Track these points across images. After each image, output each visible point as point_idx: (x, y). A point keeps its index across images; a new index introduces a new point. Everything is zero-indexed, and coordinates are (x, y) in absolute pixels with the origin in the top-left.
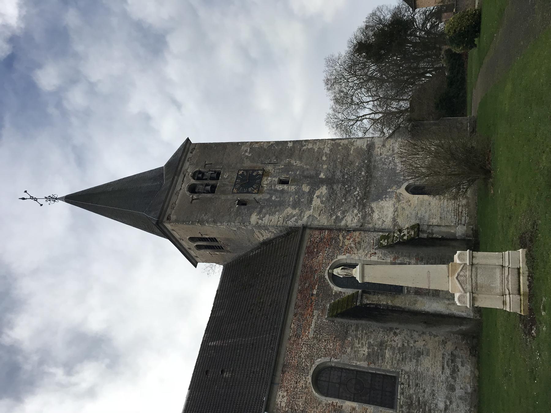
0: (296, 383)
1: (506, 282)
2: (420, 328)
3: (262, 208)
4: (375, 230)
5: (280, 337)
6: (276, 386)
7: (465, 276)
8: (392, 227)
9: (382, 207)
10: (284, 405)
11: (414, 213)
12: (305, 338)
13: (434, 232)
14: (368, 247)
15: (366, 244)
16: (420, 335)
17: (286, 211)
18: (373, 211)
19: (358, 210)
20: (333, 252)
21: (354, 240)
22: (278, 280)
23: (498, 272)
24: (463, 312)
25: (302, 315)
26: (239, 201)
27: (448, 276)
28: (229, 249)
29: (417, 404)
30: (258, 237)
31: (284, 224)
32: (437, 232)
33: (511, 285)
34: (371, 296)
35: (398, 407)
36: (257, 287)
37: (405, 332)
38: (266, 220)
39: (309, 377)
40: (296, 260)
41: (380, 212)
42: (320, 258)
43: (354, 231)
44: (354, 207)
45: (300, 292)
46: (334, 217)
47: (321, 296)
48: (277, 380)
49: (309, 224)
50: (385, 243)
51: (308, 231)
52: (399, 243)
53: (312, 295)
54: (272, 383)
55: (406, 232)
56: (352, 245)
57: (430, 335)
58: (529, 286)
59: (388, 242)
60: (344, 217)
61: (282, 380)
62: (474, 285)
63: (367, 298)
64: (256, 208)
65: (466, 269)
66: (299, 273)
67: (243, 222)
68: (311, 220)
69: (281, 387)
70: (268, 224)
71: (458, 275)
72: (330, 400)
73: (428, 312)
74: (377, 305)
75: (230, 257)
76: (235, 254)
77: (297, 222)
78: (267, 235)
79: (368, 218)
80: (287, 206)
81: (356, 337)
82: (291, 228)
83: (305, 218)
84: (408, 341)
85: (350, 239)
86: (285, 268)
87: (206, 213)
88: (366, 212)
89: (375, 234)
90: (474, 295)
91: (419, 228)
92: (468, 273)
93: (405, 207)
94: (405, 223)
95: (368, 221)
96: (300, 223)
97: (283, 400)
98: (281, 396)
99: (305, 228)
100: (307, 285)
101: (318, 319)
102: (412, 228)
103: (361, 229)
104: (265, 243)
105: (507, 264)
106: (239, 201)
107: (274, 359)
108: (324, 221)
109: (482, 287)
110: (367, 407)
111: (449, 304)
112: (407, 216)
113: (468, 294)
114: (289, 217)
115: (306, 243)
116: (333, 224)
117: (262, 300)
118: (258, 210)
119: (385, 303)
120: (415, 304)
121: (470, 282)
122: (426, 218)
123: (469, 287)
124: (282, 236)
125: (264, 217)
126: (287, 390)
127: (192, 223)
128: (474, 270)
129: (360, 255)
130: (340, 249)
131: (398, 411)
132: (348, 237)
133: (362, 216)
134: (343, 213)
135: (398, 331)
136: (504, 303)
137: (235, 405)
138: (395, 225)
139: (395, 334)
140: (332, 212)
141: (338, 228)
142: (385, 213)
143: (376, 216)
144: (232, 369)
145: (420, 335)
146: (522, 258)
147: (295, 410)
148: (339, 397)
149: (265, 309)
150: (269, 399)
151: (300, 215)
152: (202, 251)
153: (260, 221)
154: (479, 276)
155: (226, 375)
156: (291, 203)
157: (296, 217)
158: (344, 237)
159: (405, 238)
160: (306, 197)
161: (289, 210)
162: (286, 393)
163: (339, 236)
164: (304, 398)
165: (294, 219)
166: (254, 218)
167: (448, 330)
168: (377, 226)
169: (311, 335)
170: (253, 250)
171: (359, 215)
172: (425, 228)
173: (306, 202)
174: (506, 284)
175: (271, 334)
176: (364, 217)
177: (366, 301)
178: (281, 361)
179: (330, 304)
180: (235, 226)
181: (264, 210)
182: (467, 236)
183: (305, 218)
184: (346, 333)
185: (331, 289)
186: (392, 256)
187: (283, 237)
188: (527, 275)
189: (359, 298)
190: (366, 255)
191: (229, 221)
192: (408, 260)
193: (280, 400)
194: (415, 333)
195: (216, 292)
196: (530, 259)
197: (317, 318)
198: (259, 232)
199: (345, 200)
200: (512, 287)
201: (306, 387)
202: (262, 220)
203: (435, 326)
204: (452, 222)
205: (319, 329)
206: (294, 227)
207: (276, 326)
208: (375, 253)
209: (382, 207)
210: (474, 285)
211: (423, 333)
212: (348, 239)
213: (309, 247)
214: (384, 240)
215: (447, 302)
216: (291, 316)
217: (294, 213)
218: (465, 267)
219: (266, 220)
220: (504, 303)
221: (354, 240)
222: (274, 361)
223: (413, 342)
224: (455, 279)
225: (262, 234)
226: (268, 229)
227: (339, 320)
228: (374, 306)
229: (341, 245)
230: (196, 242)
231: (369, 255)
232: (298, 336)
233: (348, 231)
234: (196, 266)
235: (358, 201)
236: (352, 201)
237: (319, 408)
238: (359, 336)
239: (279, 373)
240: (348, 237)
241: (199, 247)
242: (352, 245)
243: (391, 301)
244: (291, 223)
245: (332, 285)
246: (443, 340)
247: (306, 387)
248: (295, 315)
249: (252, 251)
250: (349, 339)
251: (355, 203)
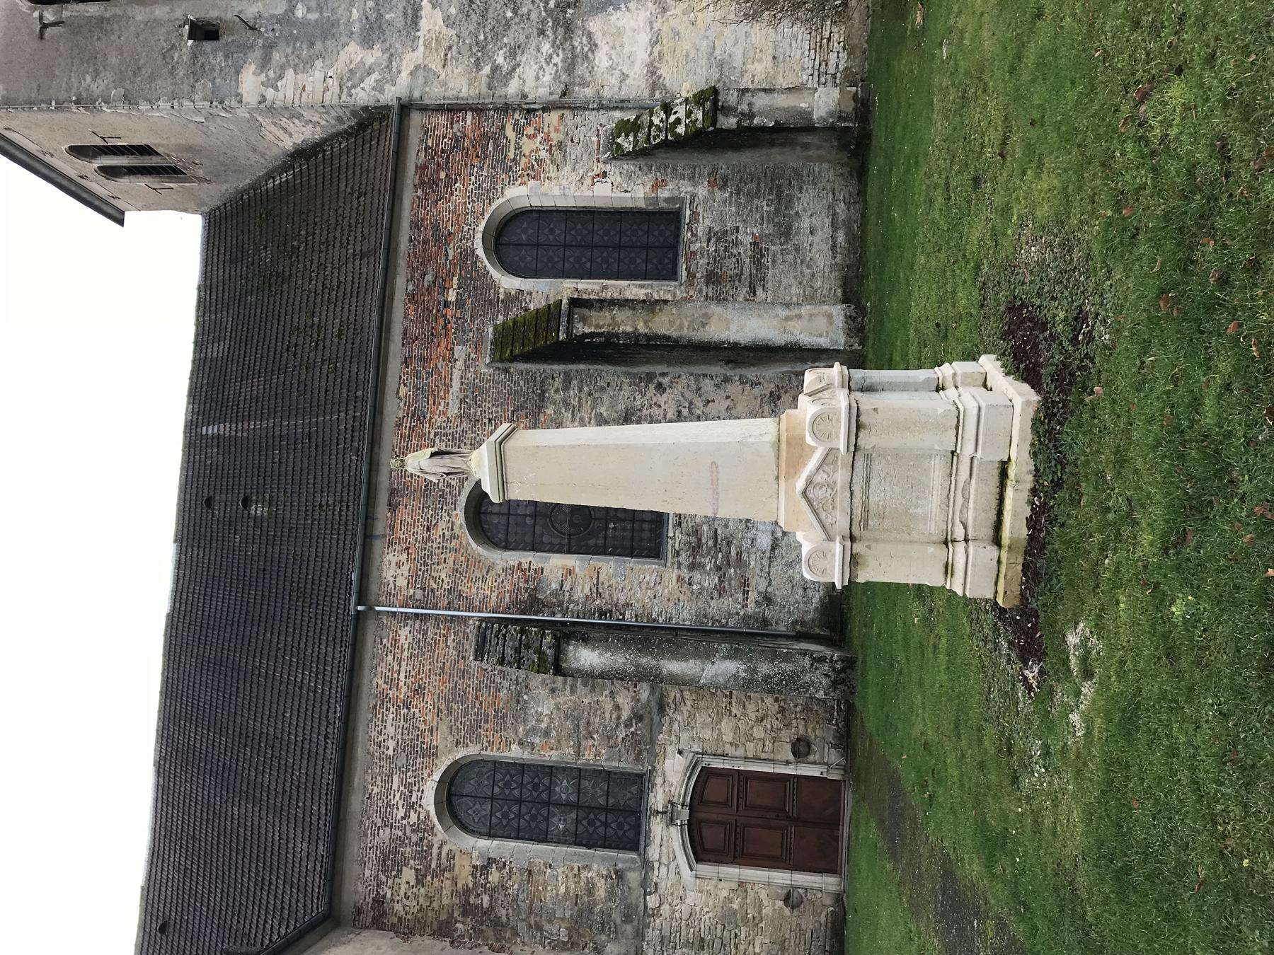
0: (428, 529)
1: (960, 501)
2: (718, 370)
3: (269, 47)
4: (603, 106)
5: (373, 424)
6: (378, 545)
7: (831, 486)
8: (646, 94)
9: (619, 33)
10: (405, 583)
11: (704, 46)
12: (438, 420)
13: (755, 109)
14: (585, 157)
15: (579, 150)
16: (717, 386)
17: (343, 56)
18: (594, 46)
19: (554, 42)
20: (493, 178)
21: (547, 139)
22: (350, 265)
23: (937, 469)
24: (820, 336)
25: (424, 360)
26: (193, 25)
27: (777, 478)
28: (200, 173)
29: (711, 543)
30: (278, 138)
31: (344, 97)
32: (767, 110)
33: (977, 513)
34: (594, 313)
35: (669, 556)
36: (300, 282)
37: (683, 381)
38: (287, 88)
39: (458, 511)
40: (392, 210)
41: (613, 48)
42: (458, 198)
43: (544, 110)
44: (542, 32)
45: (412, 298)
46: (487, 70)
47: (468, 305)
48: (380, 527)
49: (417, 94)
50: (627, 144)
51: (416, 118)
52: (665, 144)
53: (446, 304)
54: (368, 537)
55: (681, 112)
56: (543, 154)
57: (742, 383)
58: (1032, 523)
59: (636, 142)
60: (514, 69)
61: (392, 527)
62: (858, 511)
63: (584, 319)
64: (251, 47)
65: (834, 463)
66: (404, 245)
67: (217, 98)
68: (421, 80)
69: (390, 544)
70: (297, 102)
71: (809, 482)
72: (513, 558)
73: (736, 344)
74: (609, 336)
75: (216, 193)
76: (225, 186)
77: (382, 91)
78: (299, 134)
79: (581, 69)
80: (344, 39)
81: (566, 403)
82: (365, 109)
83: (404, 78)
84: (691, 403)
85: (534, 136)
86: (366, 231)
87: (97, 73)
88: (574, 48)
89: (602, 117)
90: (858, 547)
91: (715, 101)
92: (841, 476)
93: (681, 29)
94: (684, 84)
95: (582, 78)
96: (390, 95)
97: (399, 572)
98: (393, 564)
99: (405, 108)
100: (429, 278)
101: (467, 367)
102: (700, 98)
103: (564, 103)
104: (303, 154)
106: (193, 25)
107: (364, 479)
108: (458, 83)
109: (882, 517)
110: (601, 564)
111: (787, 319)
112: (687, 56)
113: (837, 548)
114: (353, 76)
115: (415, 157)
116: (484, 90)
117: (316, 319)
118: (258, 53)
119: (629, 329)
120: (704, 325)
121: (847, 504)
122: (737, 62)
123: (841, 522)
124: (346, 132)
125: (280, 78)
126: (407, 549)
127: (60, 106)
128: (860, 463)
129: (564, 182)
130: (508, 168)
131: (669, 564)
132: (530, 131)
133: (564, 61)
134: (513, 53)
135: (666, 381)
136: (948, 569)
137: (288, 584)
138: (653, 87)
139: (660, 388)
140: (480, 54)
141: (500, 102)
142: (627, 50)
143: (601, 59)
144: (267, 496)
145: (717, 386)
146: (1022, 430)
147: (433, 590)
148: (534, 547)
149: (328, 343)
150: (364, 576)
151: (389, 67)
152: (125, 182)
153: (270, 94)
154: (873, 482)
155: (257, 510)
156: (356, 28)
157: (375, 76)
158: (519, 131)
159: (681, 129)
160: (400, 7)
161: (353, 53)
162: (405, 556)
163: (503, 128)
164: (450, 561)
165: (370, 81)
166: (250, 82)
167: (785, 369)
168: (606, 93)
169: (453, 411)
170: (276, 169)
171: (556, 60)
172: (731, 98)
173: (400, 24)
174: (958, 507)
175: (351, 412)
176: (570, 67)
177: (581, 328)
178: (384, 481)
179: (495, 327)
180: (198, 111)
181: (276, 56)
182: (840, 118)
183: (404, 78)
184: (542, 396)
185: (493, 285)
186: (649, 179)
187: (350, 135)
188: (1029, 485)
189: (564, 320)
190: (581, 181)
191: (173, 97)
192: (690, 189)
194: (707, 381)
196: (1048, 430)
197: (466, 364)
198: (275, 124)
199: (515, 12)
200: (975, 519)
201: (453, 537)
202: (276, 88)
203: (753, 365)
204: (804, 69)
205: (472, 394)
206: (374, 108)
207: (359, 393)
208: (605, 174)
209: (619, 33)
210: (858, 511)
211: (727, 380)
212: (529, 137)
213: (424, 167)
214: (627, 136)
215: (783, 313)
216: (394, 366)
217: (370, 60)
218: (831, 458)
219: (287, 88)
220: (948, 569)
221: (547, 139)
222: (364, 487)
223: (701, 404)
224: (799, 497)
225: (285, 130)
226: (299, 117)
227: (522, 366)
228: (603, 339)
229: (511, 156)
230: (94, 156)
231: (588, 181)
232: (418, 416)
233: (529, 111)
234: (121, 222)
235: (550, 13)
236: (533, 16)
237: (489, 579)
238: (575, 402)
239: (382, 510)
240: (530, 131)
241: (110, 172)
242: (543, 154)
243: (645, 323)
244: (364, 96)
245: (495, 273)
246: (772, 393)
247: (453, 537)
248: (406, 362)
249: (270, 175)
250: (548, 412)
251: (544, 22)
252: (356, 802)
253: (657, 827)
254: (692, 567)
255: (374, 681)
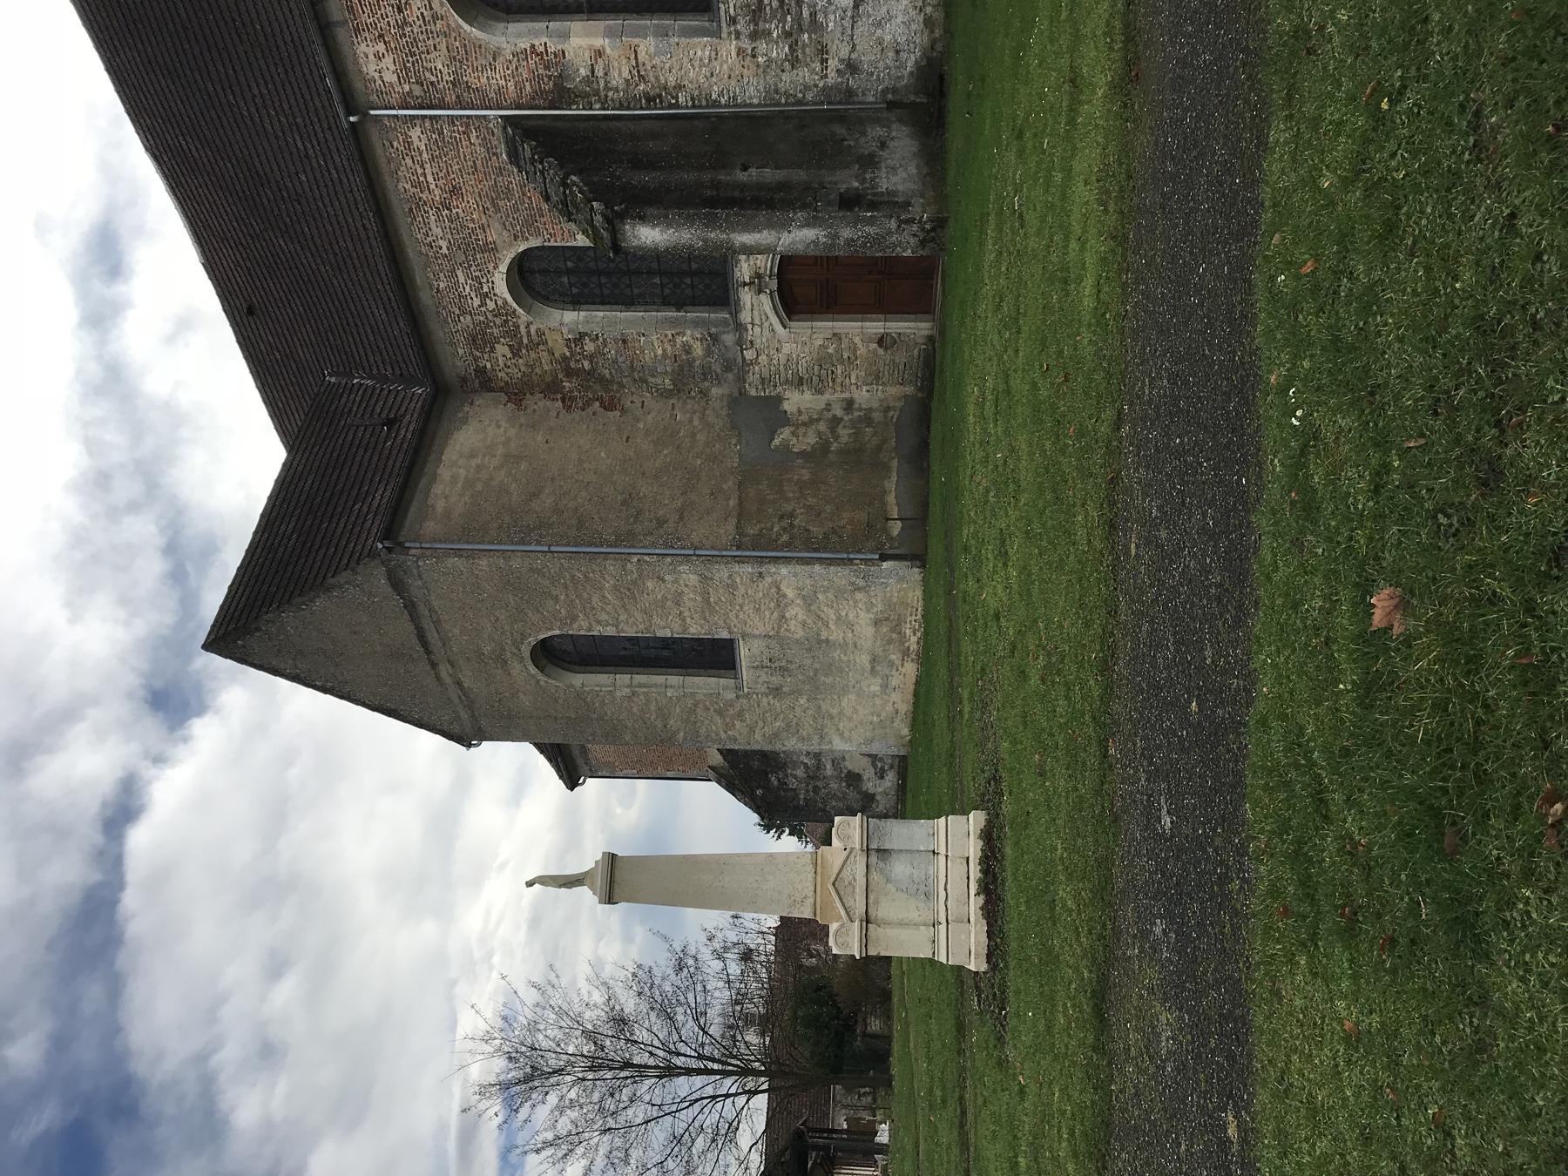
6: (341, 34)
97: (383, 65)
98: (371, 57)
105: (942, 850)
113: (857, 923)
126: (381, 36)
193: (372, 67)
195: (328, 697)
252: (425, 297)
253: (746, 296)
254: (754, 36)
255: (401, 186)
